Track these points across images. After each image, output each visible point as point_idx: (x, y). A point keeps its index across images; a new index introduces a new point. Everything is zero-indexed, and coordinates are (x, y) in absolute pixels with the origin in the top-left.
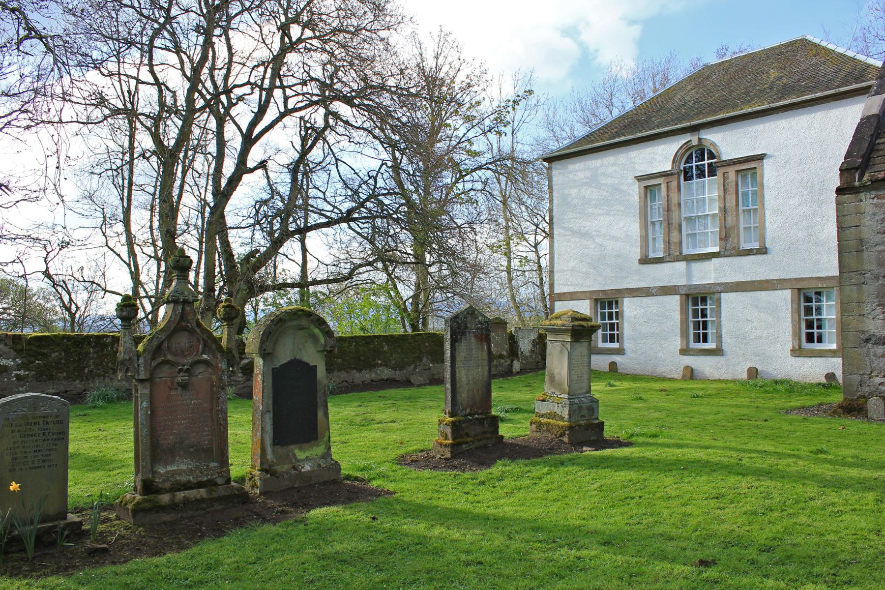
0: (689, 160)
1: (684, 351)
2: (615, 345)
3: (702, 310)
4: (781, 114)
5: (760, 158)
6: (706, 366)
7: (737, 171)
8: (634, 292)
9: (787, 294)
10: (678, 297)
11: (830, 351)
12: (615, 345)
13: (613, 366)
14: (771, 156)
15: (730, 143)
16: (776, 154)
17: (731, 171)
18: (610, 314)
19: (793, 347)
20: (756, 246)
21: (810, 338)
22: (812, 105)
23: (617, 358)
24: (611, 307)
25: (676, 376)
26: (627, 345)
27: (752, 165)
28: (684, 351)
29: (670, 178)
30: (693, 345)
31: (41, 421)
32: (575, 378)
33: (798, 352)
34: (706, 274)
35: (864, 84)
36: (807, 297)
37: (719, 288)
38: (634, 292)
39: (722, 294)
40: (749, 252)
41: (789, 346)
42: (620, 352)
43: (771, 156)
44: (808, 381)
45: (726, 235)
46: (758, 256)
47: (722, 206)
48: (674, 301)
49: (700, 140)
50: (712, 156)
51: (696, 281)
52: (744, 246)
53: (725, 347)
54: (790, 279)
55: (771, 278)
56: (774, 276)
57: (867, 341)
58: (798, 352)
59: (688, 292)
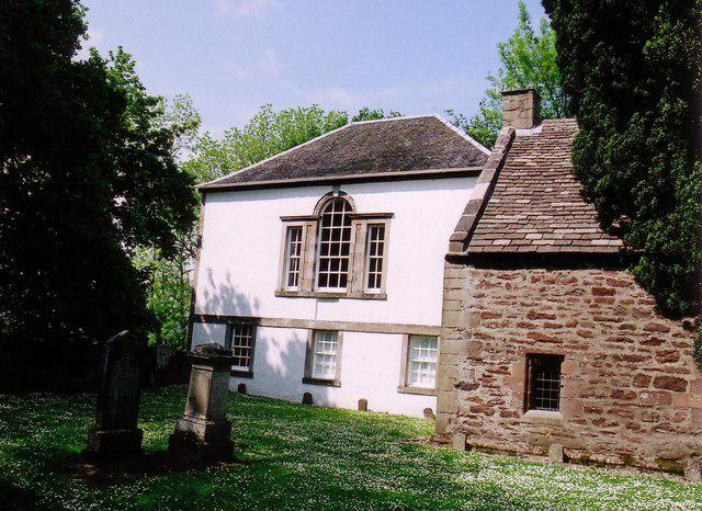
0: (329, 209)
5: (389, 216)
7: (369, 225)
12: (246, 369)
13: (242, 388)
15: (365, 200)
27: (382, 221)
29: (311, 223)
31: (295, 256)
32: (213, 402)
35: (475, 168)
36: (417, 338)
37: (342, 327)
42: (249, 375)
50: (349, 208)
51: (320, 318)
53: (343, 380)
54: (421, 326)
57: (457, 386)
59: (315, 327)
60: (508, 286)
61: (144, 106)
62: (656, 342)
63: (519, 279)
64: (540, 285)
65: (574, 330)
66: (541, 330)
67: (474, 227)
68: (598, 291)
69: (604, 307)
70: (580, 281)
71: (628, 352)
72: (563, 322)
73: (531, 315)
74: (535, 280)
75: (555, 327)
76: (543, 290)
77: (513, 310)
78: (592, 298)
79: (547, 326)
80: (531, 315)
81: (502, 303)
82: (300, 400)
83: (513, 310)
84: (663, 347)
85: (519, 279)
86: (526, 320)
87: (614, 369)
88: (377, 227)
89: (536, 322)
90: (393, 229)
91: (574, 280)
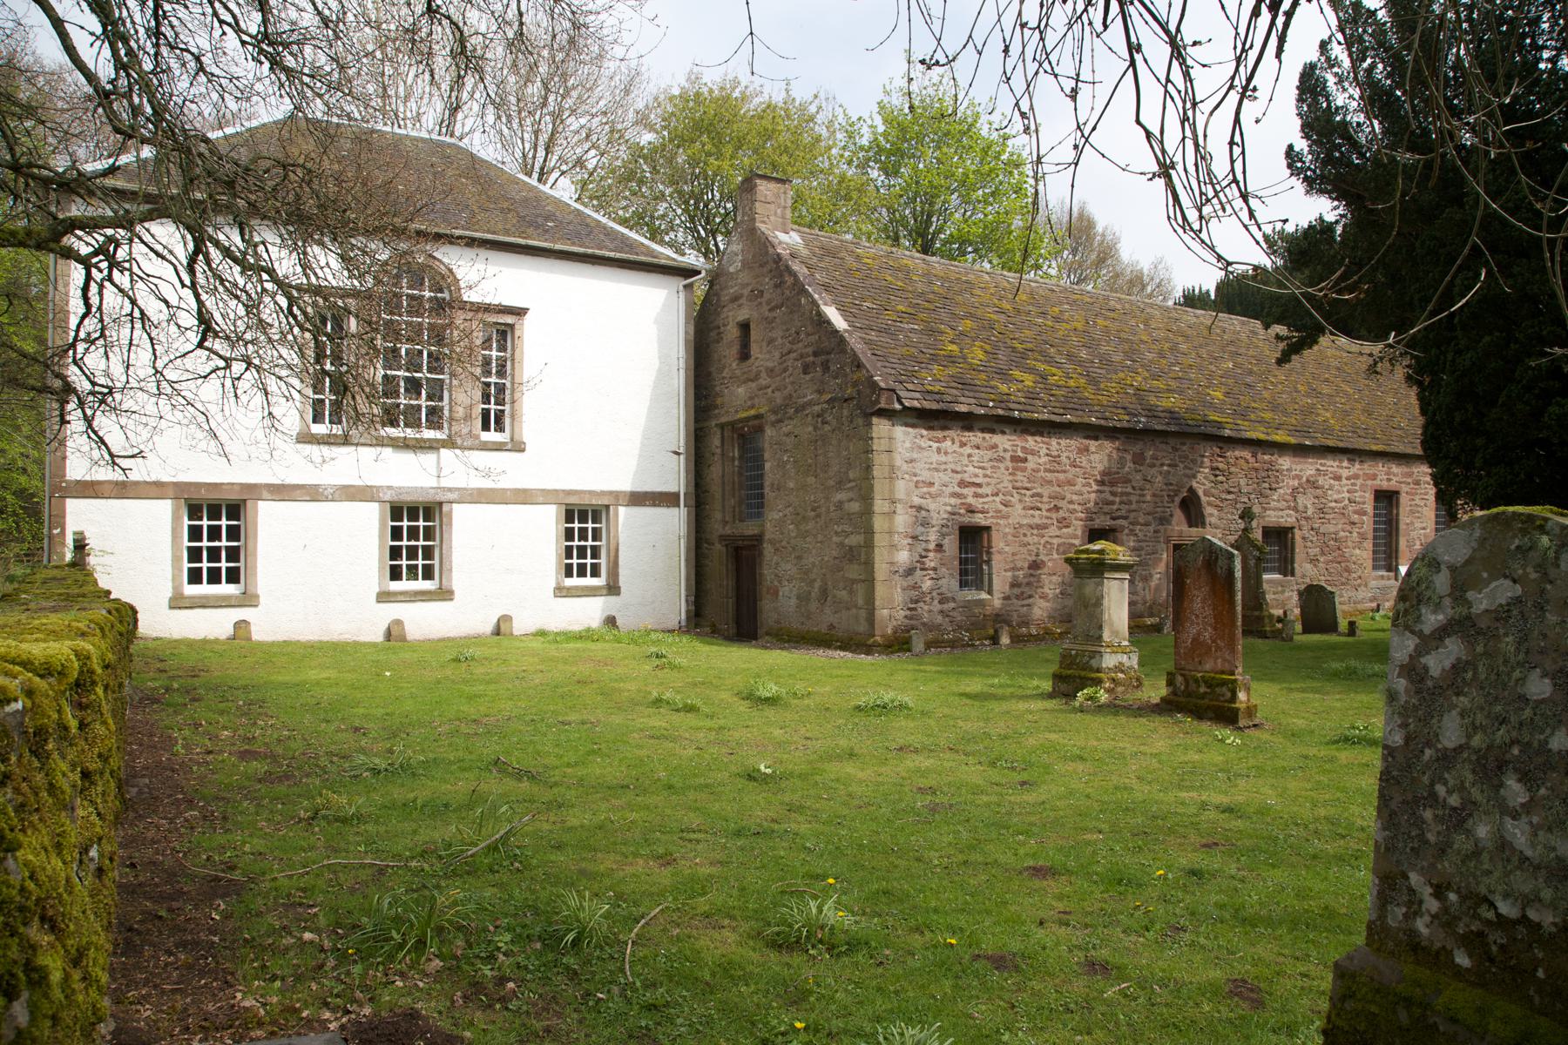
3: (594, 529)
5: (520, 312)
8: (283, 492)
27: (509, 319)
28: (384, 597)
37: (450, 496)
38: (283, 492)
60: (939, 450)
61: (1311, 227)
62: (1057, 508)
63: (949, 443)
64: (968, 450)
65: (998, 499)
66: (970, 500)
67: (121, 290)
68: (1015, 459)
69: (1020, 476)
70: (1001, 448)
71: (1037, 521)
72: (987, 490)
73: (962, 484)
74: (963, 445)
75: (981, 496)
76: (969, 456)
77: (945, 478)
78: (1009, 464)
79: (976, 495)
80: (962, 484)
81: (937, 470)
82: (378, 637)
83: (945, 478)
84: (1061, 514)
85: (949, 443)
86: (957, 489)
87: (1029, 539)
88: (503, 324)
89: (965, 491)
90: (530, 333)
91: (995, 447)
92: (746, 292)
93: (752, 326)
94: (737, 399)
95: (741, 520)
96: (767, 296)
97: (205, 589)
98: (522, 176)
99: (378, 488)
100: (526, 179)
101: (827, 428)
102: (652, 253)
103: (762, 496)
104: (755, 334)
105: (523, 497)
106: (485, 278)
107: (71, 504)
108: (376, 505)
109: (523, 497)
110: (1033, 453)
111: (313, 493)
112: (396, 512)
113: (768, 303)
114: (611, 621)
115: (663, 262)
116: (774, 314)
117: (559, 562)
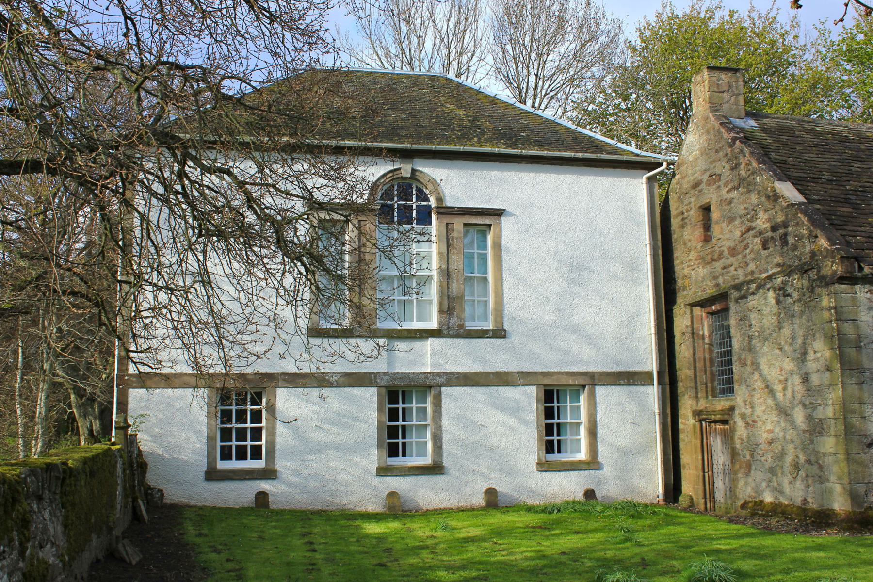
1: (383, 471)
2: (259, 464)
3: (404, 409)
4: (523, 166)
5: (498, 213)
6: (425, 493)
8: (295, 380)
9: (532, 390)
10: (533, 389)
11: (580, 462)
12: (259, 464)
14: (511, 215)
16: (517, 212)
17: (458, 223)
18: (241, 416)
19: (539, 459)
20: (490, 326)
21: (393, 451)
22: (561, 165)
23: (265, 486)
24: (242, 401)
25: (371, 508)
26: (281, 465)
27: (487, 220)
28: (383, 471)
30: (222, 465)
33: (544, 466)
34: (426, 358)
37: (438, 380)
38: (295, 380)
39: (443, 389)
40: (482, 334)
41: (533, 459)
42: (269, 474)
43: (511, 215)
44: (557, 501)
45: (450, 306)
46: (493, 340)
47: (444, 267)
48: (369, 396)
49: (414, 171)
51: (401, 369)
52: (470, 326)
55: (510, 370)
56: (513, 367)
58: (544, 466)
92: (705, 178)
93: (712, 208)
94: (695, 276)
95: (714, 396)
96: (724, 179)
97: (235, 464)
98: (518, 105)
99: (376, 375)
100: (522, 106)
101: (790, 300)
102: (615, 151)
103: (731, 372)
104: (715, 215)
105: (502, 379)
106: (457, 184)
107: (136, 395)
108: (375, 389)
109: (502, 379)
110: (690, 203)
111: (320, 381)
112: (224, 397)
113: (726, 185)
114: (590, 494)
115: (625, 158)
116: (731, 195)
117: (540, 439)
